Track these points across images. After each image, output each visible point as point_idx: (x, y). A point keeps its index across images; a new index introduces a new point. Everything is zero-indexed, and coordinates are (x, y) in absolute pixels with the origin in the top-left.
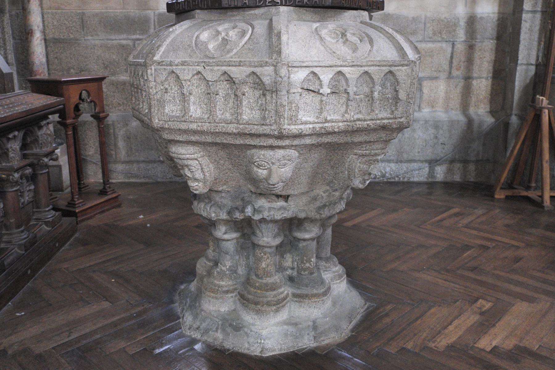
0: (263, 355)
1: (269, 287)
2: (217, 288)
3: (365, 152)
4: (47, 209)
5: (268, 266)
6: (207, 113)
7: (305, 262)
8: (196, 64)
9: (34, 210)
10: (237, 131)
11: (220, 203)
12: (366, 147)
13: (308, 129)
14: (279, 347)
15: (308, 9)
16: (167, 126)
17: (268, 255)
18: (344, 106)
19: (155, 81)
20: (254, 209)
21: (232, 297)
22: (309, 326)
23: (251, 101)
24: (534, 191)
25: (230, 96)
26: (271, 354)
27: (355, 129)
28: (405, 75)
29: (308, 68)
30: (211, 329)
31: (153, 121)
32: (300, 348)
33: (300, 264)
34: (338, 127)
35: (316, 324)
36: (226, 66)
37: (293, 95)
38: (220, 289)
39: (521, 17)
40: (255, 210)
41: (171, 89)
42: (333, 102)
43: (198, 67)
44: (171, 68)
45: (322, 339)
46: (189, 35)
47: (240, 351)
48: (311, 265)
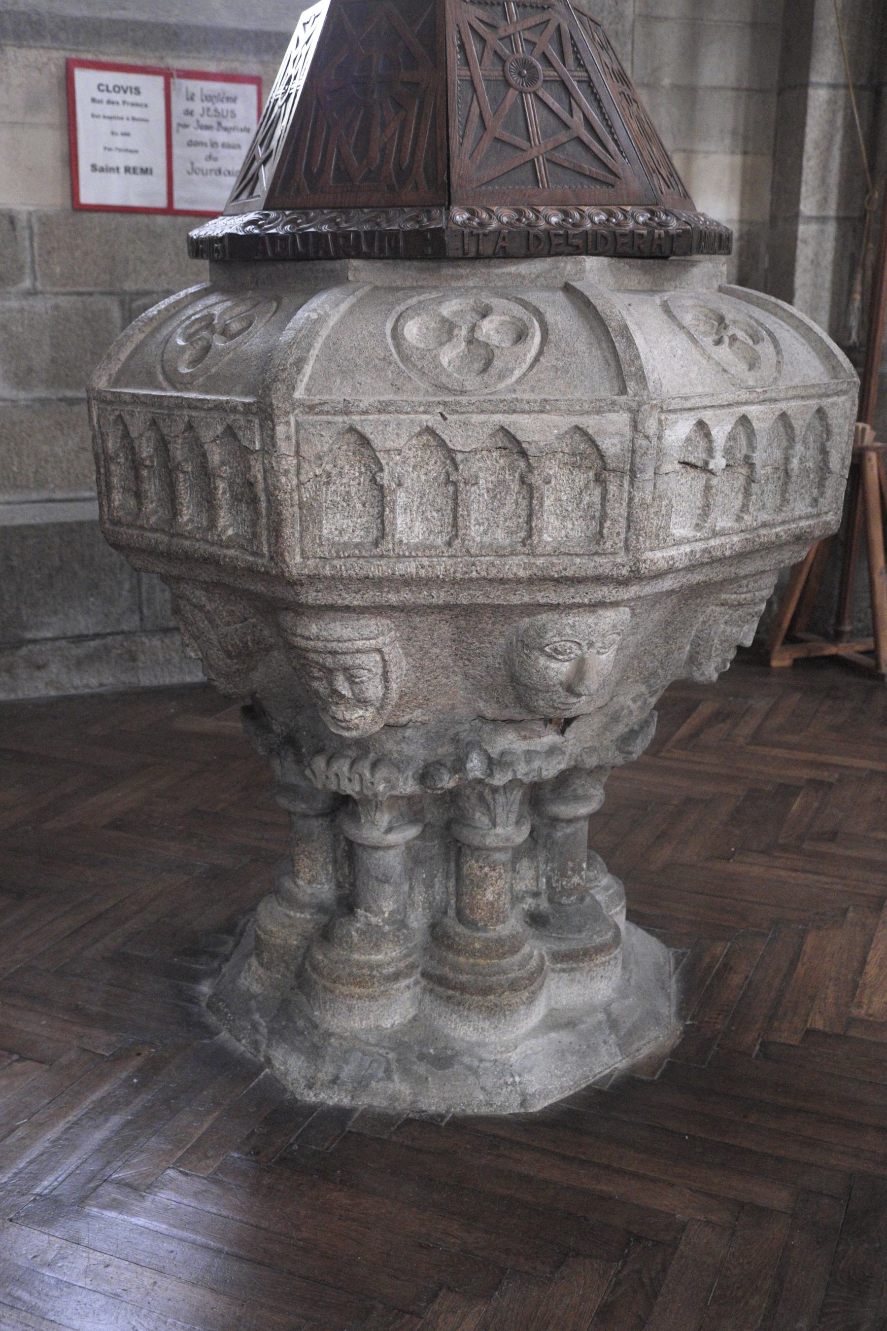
0: (531, 1111)
1: (506, 948)
3: (743, 596)
5: (499, 895)
6: (441, 532)
7: (570, 873)
8: (422, 409)
10: (529, 572)
11: (396, 755)
16: (328, 571)
17: (500, 869)
18: (740, 496)
19: (297, 453)
20: (490, 759)
21: (408, 987)
22: (600, 1023)
23: (564, 498)
24: (848, 642)
25: (509, 487)
26: (546, 1104)
29: (692, 413)
30: (372, 1076)
31: (287, 559)
32: (598, 1077)
33: (557, 881)
35: (614, 1016)
36: (505, 412)
37: (666, 478)
38: (375, 973)
39: (795, 231)
40: (492, 764)
41: (340, 474)
43: (425, 417)
44: (346, 418)
46: (370, 329)
47: (469, 1112)
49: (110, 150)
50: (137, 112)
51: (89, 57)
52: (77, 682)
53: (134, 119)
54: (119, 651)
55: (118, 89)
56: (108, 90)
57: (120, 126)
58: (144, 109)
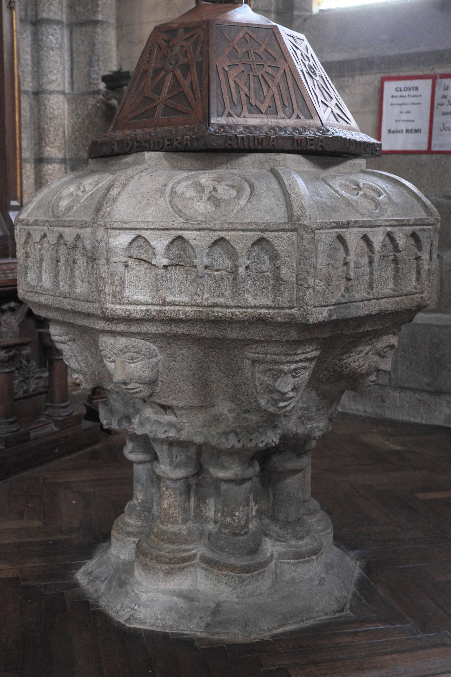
2: (122, 525)
4: (62, 405)
8: (43, 224)
9: (48, 404)
12: (256, 349)
13: (139, 312)
14: (153, 621)
15: (185, 154)
27: (213, 318)
28: (289, 245)
32: (180, 632)
34: (185, 313)
37: (115, 265)
42: (178, 278)
45: (217, 630)
48: (233, 520)
49: (399, 121)
50: (415, 100)
51: (395, 74)
52: (353, 407)
53: (413, 104)
54: (376, 395)
55: (407, 89)
56: (401, 90)
57: (405, 108)
58: (419, 98)
